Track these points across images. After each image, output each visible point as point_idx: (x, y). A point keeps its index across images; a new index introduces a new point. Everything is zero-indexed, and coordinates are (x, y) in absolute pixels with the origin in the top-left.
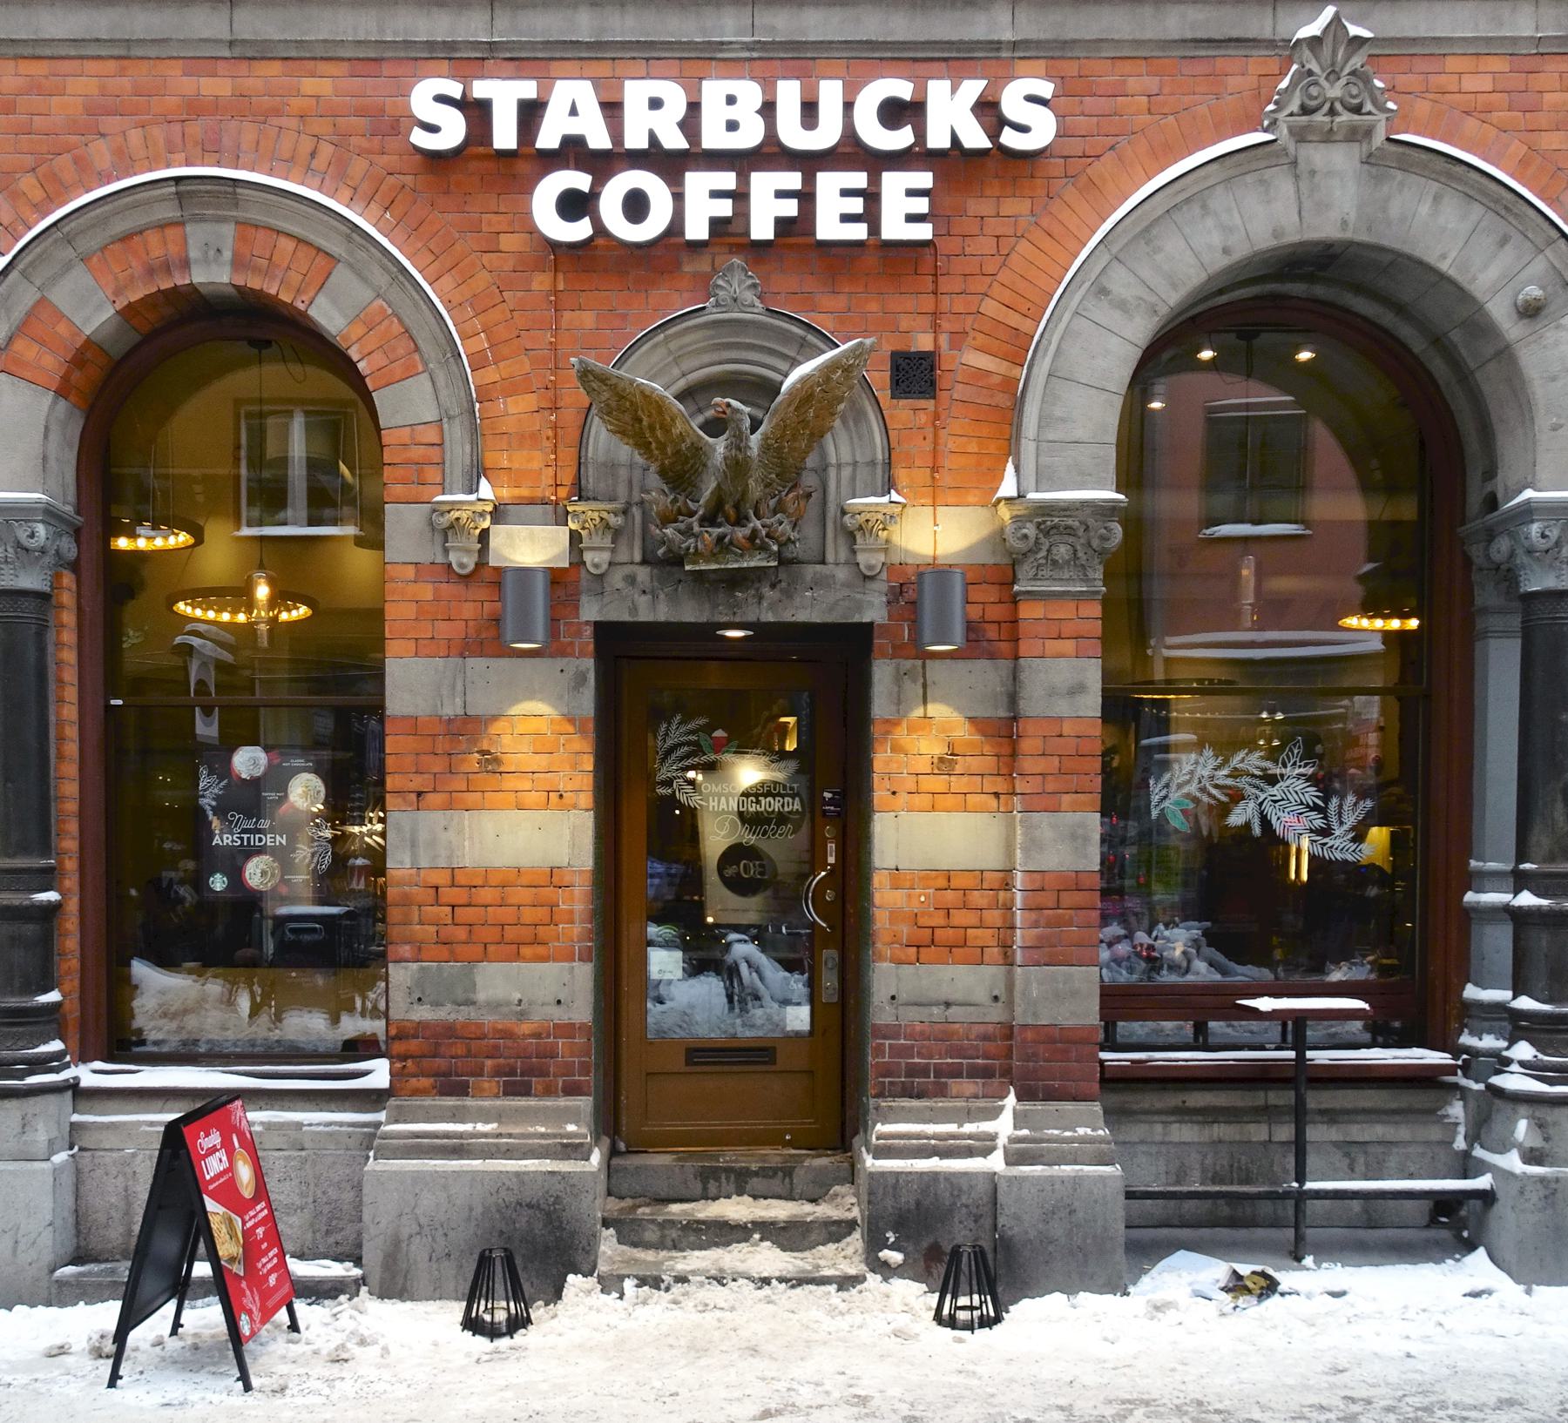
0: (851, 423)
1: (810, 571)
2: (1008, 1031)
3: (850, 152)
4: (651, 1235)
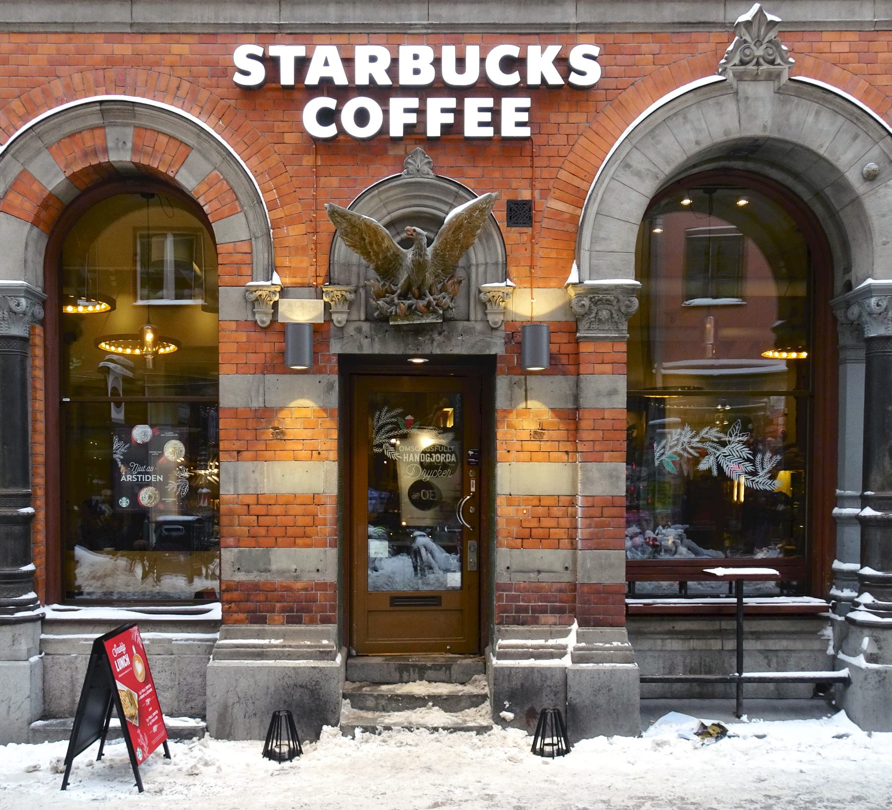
0: (484, 241)
1: (461, 325)
2: (573, 587)
3: (484, 87)
4: (370, 703)
